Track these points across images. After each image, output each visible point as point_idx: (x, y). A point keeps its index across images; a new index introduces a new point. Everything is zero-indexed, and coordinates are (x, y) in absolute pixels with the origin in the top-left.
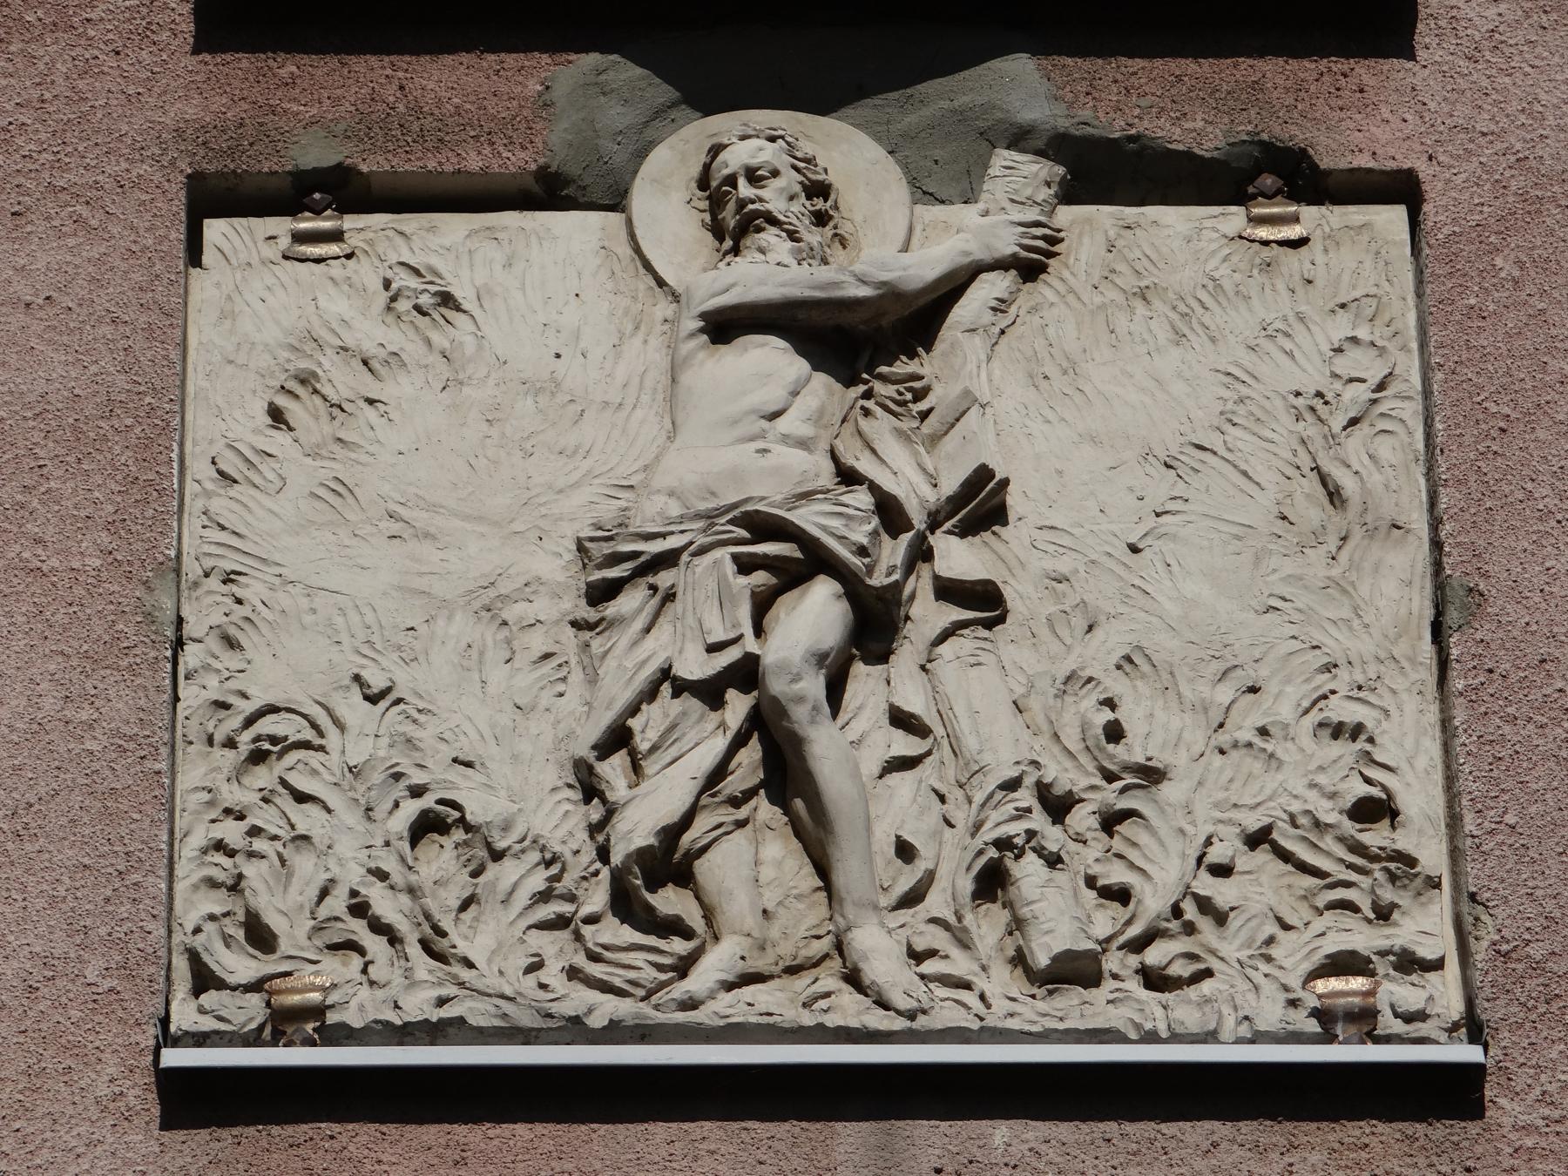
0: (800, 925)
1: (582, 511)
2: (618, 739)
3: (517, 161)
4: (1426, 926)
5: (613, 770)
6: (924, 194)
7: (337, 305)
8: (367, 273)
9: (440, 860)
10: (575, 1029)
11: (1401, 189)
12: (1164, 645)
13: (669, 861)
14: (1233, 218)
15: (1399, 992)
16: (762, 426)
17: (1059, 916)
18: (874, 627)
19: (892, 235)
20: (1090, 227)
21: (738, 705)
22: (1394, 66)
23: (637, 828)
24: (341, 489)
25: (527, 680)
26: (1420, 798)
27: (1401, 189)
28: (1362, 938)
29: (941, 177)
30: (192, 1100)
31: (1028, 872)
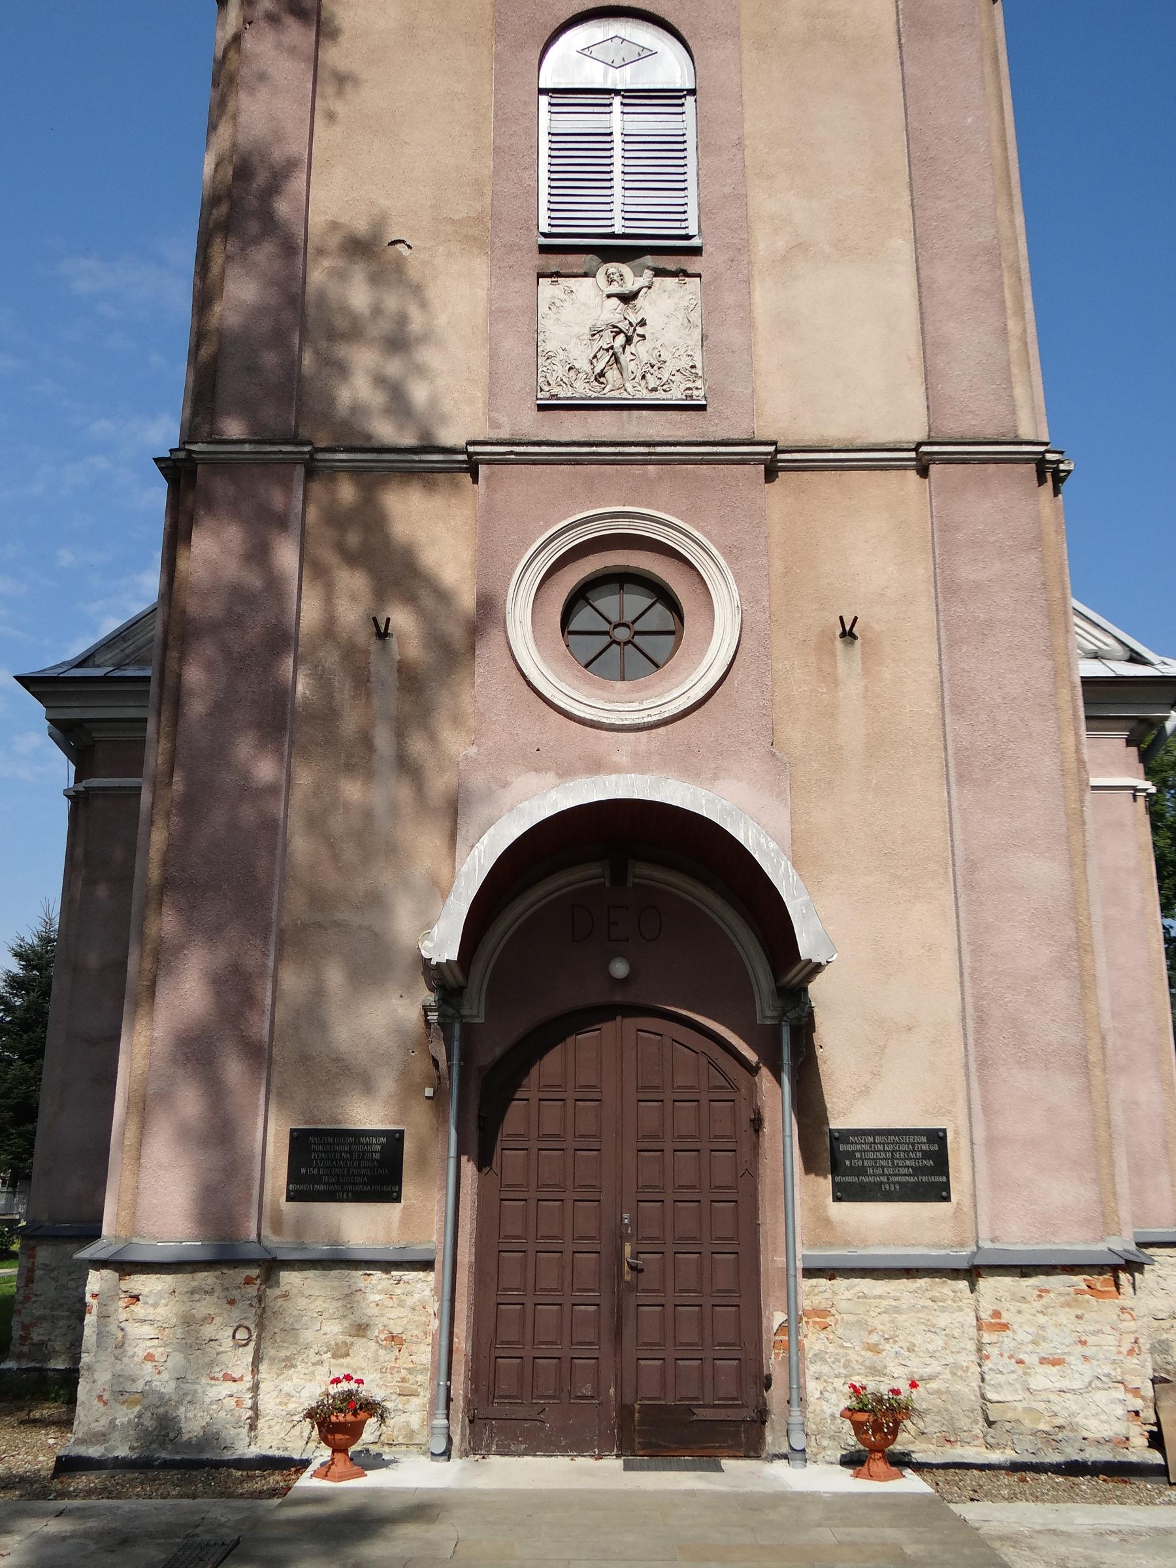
0: (619, 383)
1: (590, 323)
2: (595, 356)
3: (581, 271)
4: (699, 384)
5: (594, 361)
6: (635, 275)
7: (557, 292)
8: (561, 287)
9: (572, 373)
10: (590, 398)
11: (699, 276)
12: (666, 343)
13: (602, 374)
14: (676, 280)
15: (696, 393)
16: (613, 311)
17: (652, 382)
18: (629, 340)
19: (632, 282)
20: (658, 280)
21: (611, 352)
22: (699, 258)
23: (597, 370)
24: (558, 319)
25: (584, 348)
26: (699, 365)
27: (699, 276)
28: (691, 385)
29: (638, 274)
30: (542, 408)
31: (648, 376)
